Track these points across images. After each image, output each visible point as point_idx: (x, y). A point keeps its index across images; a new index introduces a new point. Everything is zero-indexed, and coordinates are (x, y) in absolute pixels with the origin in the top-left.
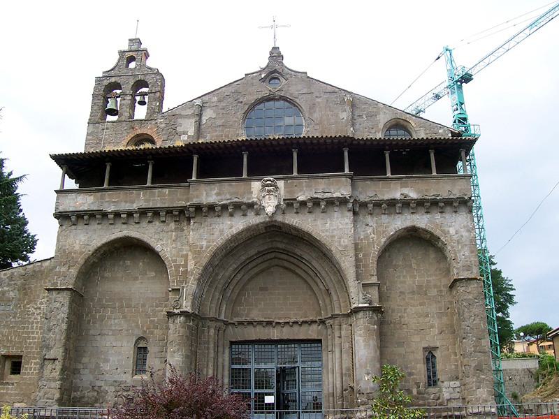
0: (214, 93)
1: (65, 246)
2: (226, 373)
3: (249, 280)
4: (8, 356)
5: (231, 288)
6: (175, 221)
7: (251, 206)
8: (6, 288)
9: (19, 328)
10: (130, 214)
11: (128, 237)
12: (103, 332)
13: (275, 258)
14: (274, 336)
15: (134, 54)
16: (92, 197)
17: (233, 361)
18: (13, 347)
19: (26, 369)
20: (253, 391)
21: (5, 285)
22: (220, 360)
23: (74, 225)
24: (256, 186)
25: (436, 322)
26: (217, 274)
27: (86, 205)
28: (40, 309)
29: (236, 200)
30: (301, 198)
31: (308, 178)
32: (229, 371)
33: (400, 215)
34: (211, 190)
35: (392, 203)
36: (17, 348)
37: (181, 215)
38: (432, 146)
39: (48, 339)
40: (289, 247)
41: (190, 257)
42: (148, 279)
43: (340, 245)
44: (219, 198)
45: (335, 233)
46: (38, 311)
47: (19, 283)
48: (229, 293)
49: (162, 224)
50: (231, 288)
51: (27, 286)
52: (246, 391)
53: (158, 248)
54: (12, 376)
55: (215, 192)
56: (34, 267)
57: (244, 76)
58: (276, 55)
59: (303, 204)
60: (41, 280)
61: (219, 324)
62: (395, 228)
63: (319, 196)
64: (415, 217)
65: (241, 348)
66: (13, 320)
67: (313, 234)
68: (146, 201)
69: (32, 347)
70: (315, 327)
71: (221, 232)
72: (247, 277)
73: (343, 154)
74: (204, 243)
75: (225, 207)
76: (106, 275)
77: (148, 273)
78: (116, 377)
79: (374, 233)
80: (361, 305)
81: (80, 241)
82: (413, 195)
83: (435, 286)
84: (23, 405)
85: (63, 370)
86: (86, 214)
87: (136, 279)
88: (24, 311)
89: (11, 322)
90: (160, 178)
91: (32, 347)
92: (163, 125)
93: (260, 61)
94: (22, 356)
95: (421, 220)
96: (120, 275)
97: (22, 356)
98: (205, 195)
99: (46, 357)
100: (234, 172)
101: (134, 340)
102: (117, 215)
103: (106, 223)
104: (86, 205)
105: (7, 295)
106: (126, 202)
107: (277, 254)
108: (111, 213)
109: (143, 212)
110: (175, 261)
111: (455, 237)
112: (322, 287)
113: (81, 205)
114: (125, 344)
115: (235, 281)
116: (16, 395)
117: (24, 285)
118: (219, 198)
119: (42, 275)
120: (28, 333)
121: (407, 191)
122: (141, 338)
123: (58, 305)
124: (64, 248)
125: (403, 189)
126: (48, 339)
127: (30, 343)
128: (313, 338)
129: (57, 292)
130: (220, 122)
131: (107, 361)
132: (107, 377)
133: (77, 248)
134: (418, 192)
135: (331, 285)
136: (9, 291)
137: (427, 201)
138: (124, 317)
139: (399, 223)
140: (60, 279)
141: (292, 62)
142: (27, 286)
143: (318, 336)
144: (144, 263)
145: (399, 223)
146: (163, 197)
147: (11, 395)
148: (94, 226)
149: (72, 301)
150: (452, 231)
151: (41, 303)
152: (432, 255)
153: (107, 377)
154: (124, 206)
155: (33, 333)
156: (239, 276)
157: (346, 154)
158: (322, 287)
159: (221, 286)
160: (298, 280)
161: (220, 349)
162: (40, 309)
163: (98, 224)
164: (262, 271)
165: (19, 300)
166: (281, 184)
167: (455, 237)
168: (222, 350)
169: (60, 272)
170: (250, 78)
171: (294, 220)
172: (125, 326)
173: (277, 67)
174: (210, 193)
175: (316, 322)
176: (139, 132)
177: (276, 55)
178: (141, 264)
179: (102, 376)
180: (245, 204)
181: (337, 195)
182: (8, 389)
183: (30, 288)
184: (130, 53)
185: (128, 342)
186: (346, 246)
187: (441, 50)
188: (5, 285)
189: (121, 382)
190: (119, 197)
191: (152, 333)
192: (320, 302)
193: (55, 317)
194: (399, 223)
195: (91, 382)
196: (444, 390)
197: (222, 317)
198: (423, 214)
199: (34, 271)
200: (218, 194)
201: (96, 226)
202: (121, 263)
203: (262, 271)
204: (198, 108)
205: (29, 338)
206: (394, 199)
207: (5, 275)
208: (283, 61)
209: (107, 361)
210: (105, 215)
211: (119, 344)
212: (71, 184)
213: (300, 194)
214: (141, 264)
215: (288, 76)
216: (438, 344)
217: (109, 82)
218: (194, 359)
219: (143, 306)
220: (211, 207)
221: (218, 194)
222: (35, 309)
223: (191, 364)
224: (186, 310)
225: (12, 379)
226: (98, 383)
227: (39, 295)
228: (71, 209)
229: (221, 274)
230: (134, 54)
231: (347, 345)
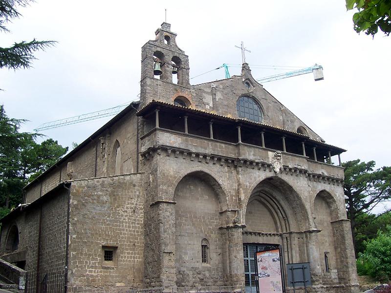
0: (220, 82)
4: (106, 246)
6: (228, 166)
7: (269, 166)
8: (100, 193)
9: (113, 225)
10: (205, 156)
11: (202, 172)
12: (182, 234)
15: (166, 34)
16: (180, 139)
18: (111, 239)
19: (122, 257)
21: (99, 190)
24: (271, 154)
25: (327, 239)
27: (177, 143)
28: (127, 212)
29: (263, 161)
30: (290, 166)
31: (292, 155)
36: (114, 241)
37: (234, 163)
38: (332, 150)
39: (165, 238)
40: (271, 191)
42: (205, 200)
44: (254, 157)
45: (302, 188)
46: (126, 214)
47: (109, 190)
49: (221, 167)
51: (115, 193)
52: (250, 276)
54: (106, 262)
56: (119, 179)
59: (290, 169)
60: (125, 190)
64: (325, 185)
67: (293, 187)
68: (214, 150)
69: (124, 241)
70: (277, 237)
74: (248, 184)
75: (257, 164)
76: (179, 194)
78: (193, 265)
81: (173, 169)
82: (326, 174)
83: (326, 221)
84: (122, 284)
87: (198, 199)
88: (115, 213)
89: (107, 220)
91: (124, 241)
92: (195, 95)
94: (117, 247)
96: (188, 195)
97: (117, 247)
98: (247, 154)
99: (165, 251)
101: (201, 240)
102: (197, 155)
103: (188, 160)
104: (177, 143)
105: (101, 198)
106: (202, 147)
108: (194, 153)
113: (174, 142)
116: (116, 277)
117: (113, 192)
118: (254, 157)
119: (125, 186)
120: (120, 230)
121: (323, 171)
122: (205, 239)
123: (168, 214)
124: (163, 172)
126: (165, 238)
127: (122, 238)
129: (167, 204)
130: (226, 103)
131: (186, 254)
132: (187, 264)
133: (172, 173)
134: (328, 173)
136: (102, 195)
138: (194, 224)
139: (320, 187)
142: (115, 193)
144: (201, 189)
146: (223, 149)
147: (113, 277)
148: (181, 159)
151: (127, 208)
152: (324, 205)
153: (187, 264)
154: (201, 151)
155: (123, 230)
157: (186, 119)
160: (265, 210)
162: (127, 212)
163: (184, 159)
169: (163, 189)
170: (237, 79)
172: (195, 231)
174: (250, 153)
176: (181, 94)
178: (199, 189)
179: (184, 264)
181: (303, 168)
182: (110, 272)
183: (118, 195)
185: (197, 241)
186: (306, 197)
187: (222, 65)
189: (196, 268)
190: (197, 143)
191: (210, 236)
193: (168, 222)
194: (196, 167)
195: (178, 268)
196: (332, 274)
199: (119, 182)
200: (254, 155)
201: (182, 160)
202: (188, 187)
204: (212, 88)
205: (121, 234)
209: (186, 254)
210: (190, 154)
214: (199, 189)
216: (329, 251)
219: (204, 218)
220: (251, 163)
222: (124, 212)
224: (243, 224)
225: (106, 264)
226: (183, 269)
227: (125, 202)
228: (168, 144)
230: (166, 34)
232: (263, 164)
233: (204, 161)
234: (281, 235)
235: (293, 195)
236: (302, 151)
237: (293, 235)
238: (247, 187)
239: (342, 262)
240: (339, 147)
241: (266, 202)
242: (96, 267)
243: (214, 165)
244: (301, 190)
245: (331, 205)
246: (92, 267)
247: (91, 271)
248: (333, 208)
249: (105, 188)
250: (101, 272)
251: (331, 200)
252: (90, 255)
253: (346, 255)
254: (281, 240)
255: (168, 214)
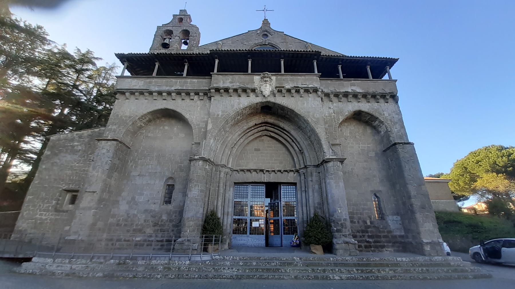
1: (119, 112)
2: (231, 205)
3: (248, 143)
5: (236, 147)
7: (253, 90)
10: (169, 93)
13: (266, 130)
14: (264, 179)
16: (143, 82)
17: (236, 196)
20: (290, 227)
22: (227, 195)
23: (127, 99)
24: (257, 78)
26: (227, 137)
30: (288, 87)
32: (232, 203)
33: (350, 103)
34: (226, 80)
35: (346, 95)
41: (209, 121)
43: (314, 118)
48: (235, 151)
50: (236, 147)
53: (187, 116)
55: (229, 81)
57: (247, 32)
58: (266, 22)
59: (289, 91)
61: (227, 170)
62: (348, 111)
63: (300, 86)
65: (242, 187)
66: (77, 165)
70: (291, 174)
71: (233, 106)
72: (246, 142)
73: (313, 64)
77: (179, 135)
79: (334, 113)
80: (331, 157)
82: (359, 90)
85: (100, 201)
86: (137, 92)
90: (192, 73)
93: (257, 25)
95: (364, 106)
100: (243, 70)
102: (160, 93)
103: (150, 98)
105: (76, 148)
107: (266, 127)
108: (155, 92)
109: (179, 93)
110: (199, 125)
111: (389, 118)
112: (296, 148)
114: (157, 182)
115: (239, 143)
121: (354, 88)
122: (171, 178)
125: (352, 87)
128: (291, 182)
135: (303, 147)
136: (78, 145)
137: (369, 94)
140: (111, 134)
141: (274, 26)
143: (294, 181)
145: (353, 106)
148: (142, 99)
149: (117, 151)
150: (386, 114)
152: (369, 130)
156: (242, 140)
158: (296, 148)
159: (230, 145)
161: (228, 188)
164: (256, 138)
165: (85, 151)
166: (274, 78)
167: (389, 118)
168: (228, 188)
171: (281, 100)
173: (267, 28)
175: (293, 171)
177: (266, 22)
180: (249, 89)
184: (180, 16)
188: (76, 141)
189: (151, 211)
192: (295, 159)
197: (230, 166)
198: (366, 103)
202: (161, 128)
203: (256, 138)
206: (348, 92)
207: (76, 134)
208: (271, 26)
210: (151, 93)
211: (152, 182)
212: (127, 73)
213: (286, 85)
214: (175, 129)
215: (273, 33)
217: (165, 29)
218: (208, 193)
221: (231, 82)
223: (205, 197)
229: (230, 138)
231: (317, 187)
232: (245, 90)
233: (169, 98)
234: (297, 171)
235: (301, 121)
236: (338, 73)
237: (309, 170)
238: (218, 115)
239: (404, 204)
240: (391, 57)
241: (280, 139)
242: (48, 211)
243: (183, 101)
244: (309, 112)
245: (380, 129)
246: (44, 211)
247: (41, 215)
248: (382, 133)
249: (82, 139)
250: (52, 215)
251: (377, 122)
252: (46, 199)
253: (408, 193)
254: (299, 178)
255: (104, 151)
